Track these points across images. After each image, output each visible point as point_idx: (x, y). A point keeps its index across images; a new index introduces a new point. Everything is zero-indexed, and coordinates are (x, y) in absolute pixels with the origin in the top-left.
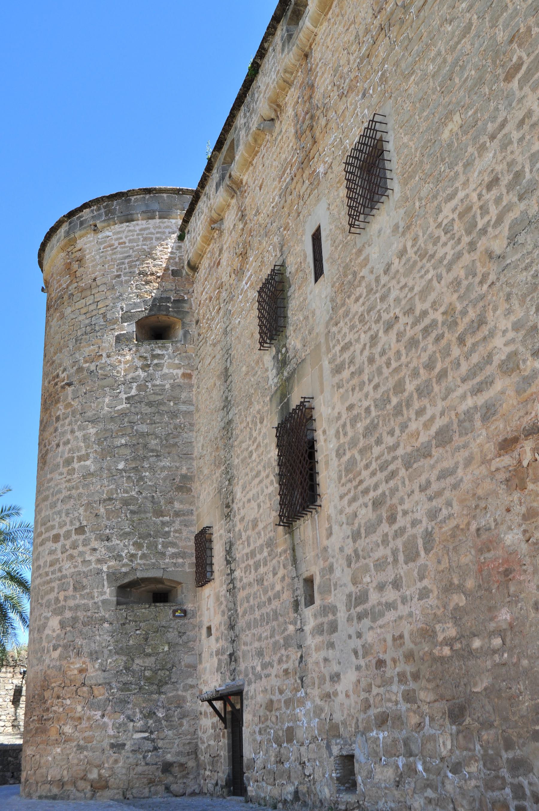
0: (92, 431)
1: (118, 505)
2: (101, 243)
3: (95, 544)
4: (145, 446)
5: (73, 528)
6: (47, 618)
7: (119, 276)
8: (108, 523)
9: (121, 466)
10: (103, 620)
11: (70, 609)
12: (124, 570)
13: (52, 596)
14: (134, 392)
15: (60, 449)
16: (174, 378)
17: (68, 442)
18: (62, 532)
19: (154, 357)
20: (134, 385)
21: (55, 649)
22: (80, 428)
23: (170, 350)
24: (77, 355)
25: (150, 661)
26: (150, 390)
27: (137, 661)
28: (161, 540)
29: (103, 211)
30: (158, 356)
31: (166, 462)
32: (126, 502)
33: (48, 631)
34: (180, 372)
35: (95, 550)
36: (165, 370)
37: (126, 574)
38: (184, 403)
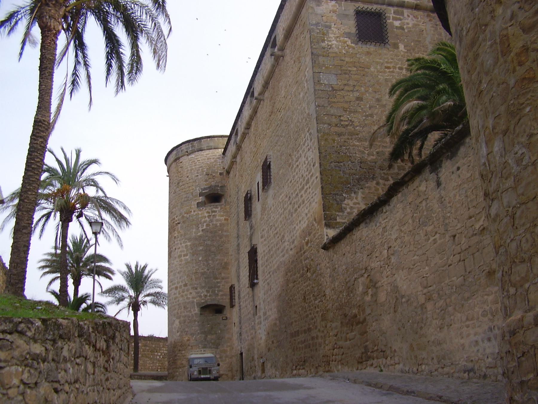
0: (189, 244)
1: (200, 275)
2: (190, 161)
3: (191, 291)
4: (210, 250)
5: (183, 284)
6: (174, 321)
7: (198, 176)
8: (196, 282)
9: (200, 259)
10: (195, 321)
11: (183, 317)
12: (203, 301)
13: (176, 311)
14: (205, 227)
15: (177, 251)
16: (220, 220)
17: (179, 248)
18: (178, 286)
19: (213, 212)
20: (205, 224)
21: (178, 332)
22: (184, 242)
23: (219, 208)
24: (182, 210)
25: (214, 337)
26: (211, 226)
27: (209, 336)
28: (217, 289)
29: (190, 145)
30: (215, 212)
31: (218, 257)
32: (203, 274)
33: (175, 325)
34: (223, 218)
35: (191, 293)
36: (217, 217)
37: (203, 303)
38: (226, 231)
